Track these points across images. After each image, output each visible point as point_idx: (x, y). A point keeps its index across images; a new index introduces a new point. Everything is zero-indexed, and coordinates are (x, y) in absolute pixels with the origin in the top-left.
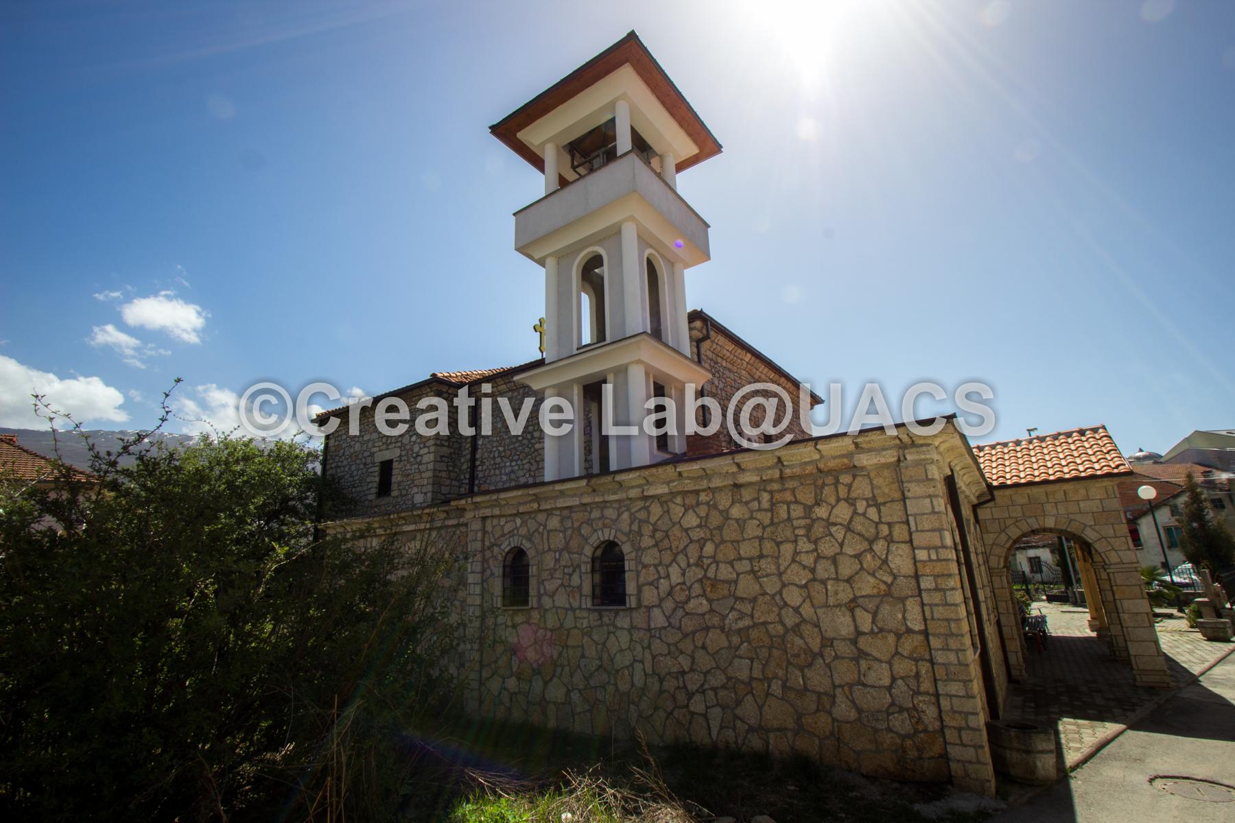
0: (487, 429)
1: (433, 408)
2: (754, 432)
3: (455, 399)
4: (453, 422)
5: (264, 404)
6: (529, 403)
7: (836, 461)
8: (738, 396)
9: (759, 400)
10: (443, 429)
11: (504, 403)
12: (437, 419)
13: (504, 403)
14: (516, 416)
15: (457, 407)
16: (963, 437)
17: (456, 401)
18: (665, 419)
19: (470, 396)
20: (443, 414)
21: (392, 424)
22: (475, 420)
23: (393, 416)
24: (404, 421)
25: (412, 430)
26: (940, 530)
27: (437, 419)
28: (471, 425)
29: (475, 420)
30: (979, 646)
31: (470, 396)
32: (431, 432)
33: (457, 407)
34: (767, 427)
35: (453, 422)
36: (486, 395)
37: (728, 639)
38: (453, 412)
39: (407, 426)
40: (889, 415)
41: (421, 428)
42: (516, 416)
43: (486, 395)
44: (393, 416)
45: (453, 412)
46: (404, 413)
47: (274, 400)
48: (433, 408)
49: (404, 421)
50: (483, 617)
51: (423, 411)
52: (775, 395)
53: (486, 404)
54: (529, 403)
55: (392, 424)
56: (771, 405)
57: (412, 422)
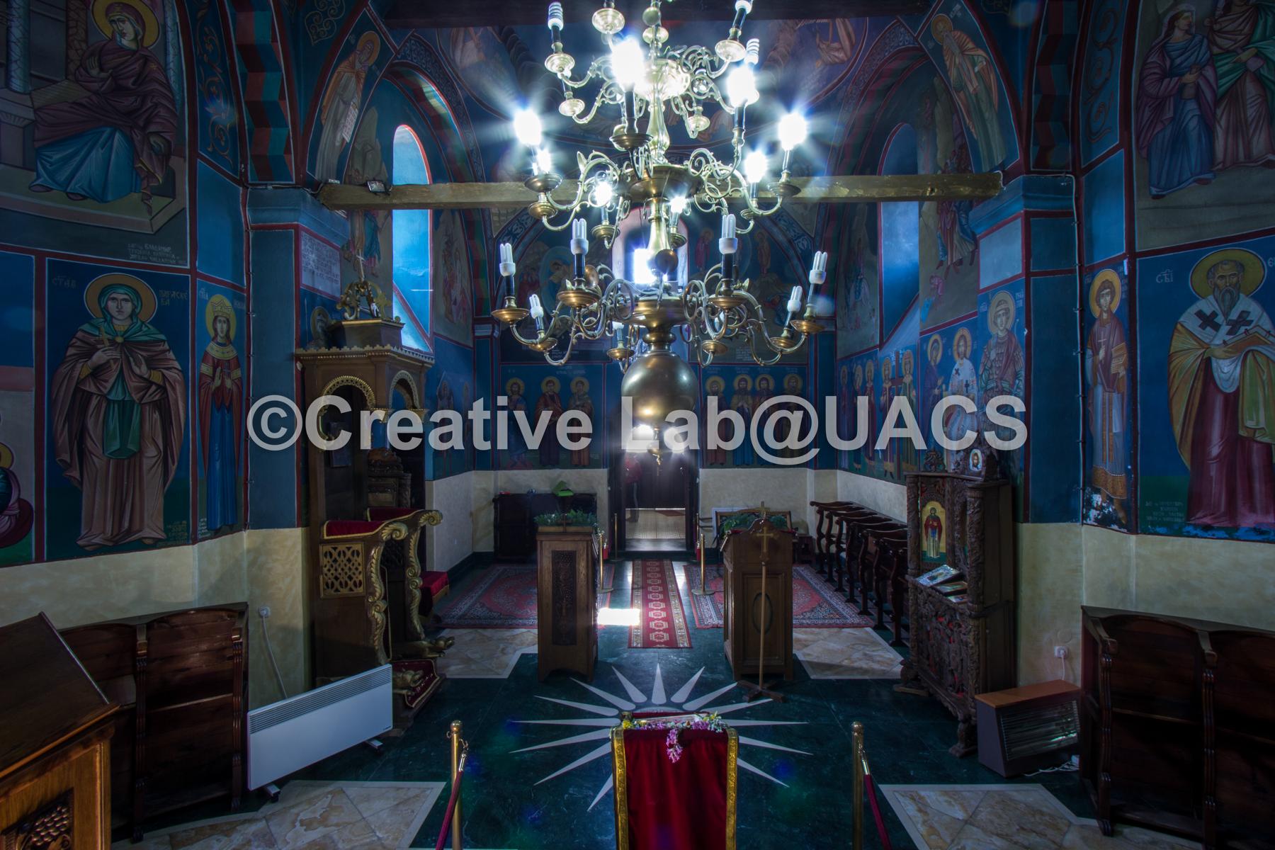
0: (502, 444)
1: (446, 422)
3: (470, 413)
5: (274, 417)
6: (545, 416)
7: (418, 593)
8: (766, 405)
9: (784, 413)
10: (457, 443)
11: (520, 416)
12: (451, 433)
13: (520, 416)
14: (533, 428)
15: (472, 420)
19: (485, 409)
20: (457, 428)
21: (574, 438)
22: (490, 431)
23: (575, 430)
24: (587, 435)
27: (451, 433)
28: (486, 439)
29: (490, 431)
30: (339, 379)
31: (485, 409)
32: (445, 446)
33: (472, 420)
34: (792, 442)
36: (503, 408)
37: (1232, 261)
41: (434, 441)
42: (533, 428)
43: (503, 408)
44: (575, 430)
47: (283, 414)
48: (446, 422)
49: (587, 435)
50: (1113, 480)
51: (436, 425)
52: (799, 407)
53: (502, 417)
55: (574, 438)
56: (796, 418)
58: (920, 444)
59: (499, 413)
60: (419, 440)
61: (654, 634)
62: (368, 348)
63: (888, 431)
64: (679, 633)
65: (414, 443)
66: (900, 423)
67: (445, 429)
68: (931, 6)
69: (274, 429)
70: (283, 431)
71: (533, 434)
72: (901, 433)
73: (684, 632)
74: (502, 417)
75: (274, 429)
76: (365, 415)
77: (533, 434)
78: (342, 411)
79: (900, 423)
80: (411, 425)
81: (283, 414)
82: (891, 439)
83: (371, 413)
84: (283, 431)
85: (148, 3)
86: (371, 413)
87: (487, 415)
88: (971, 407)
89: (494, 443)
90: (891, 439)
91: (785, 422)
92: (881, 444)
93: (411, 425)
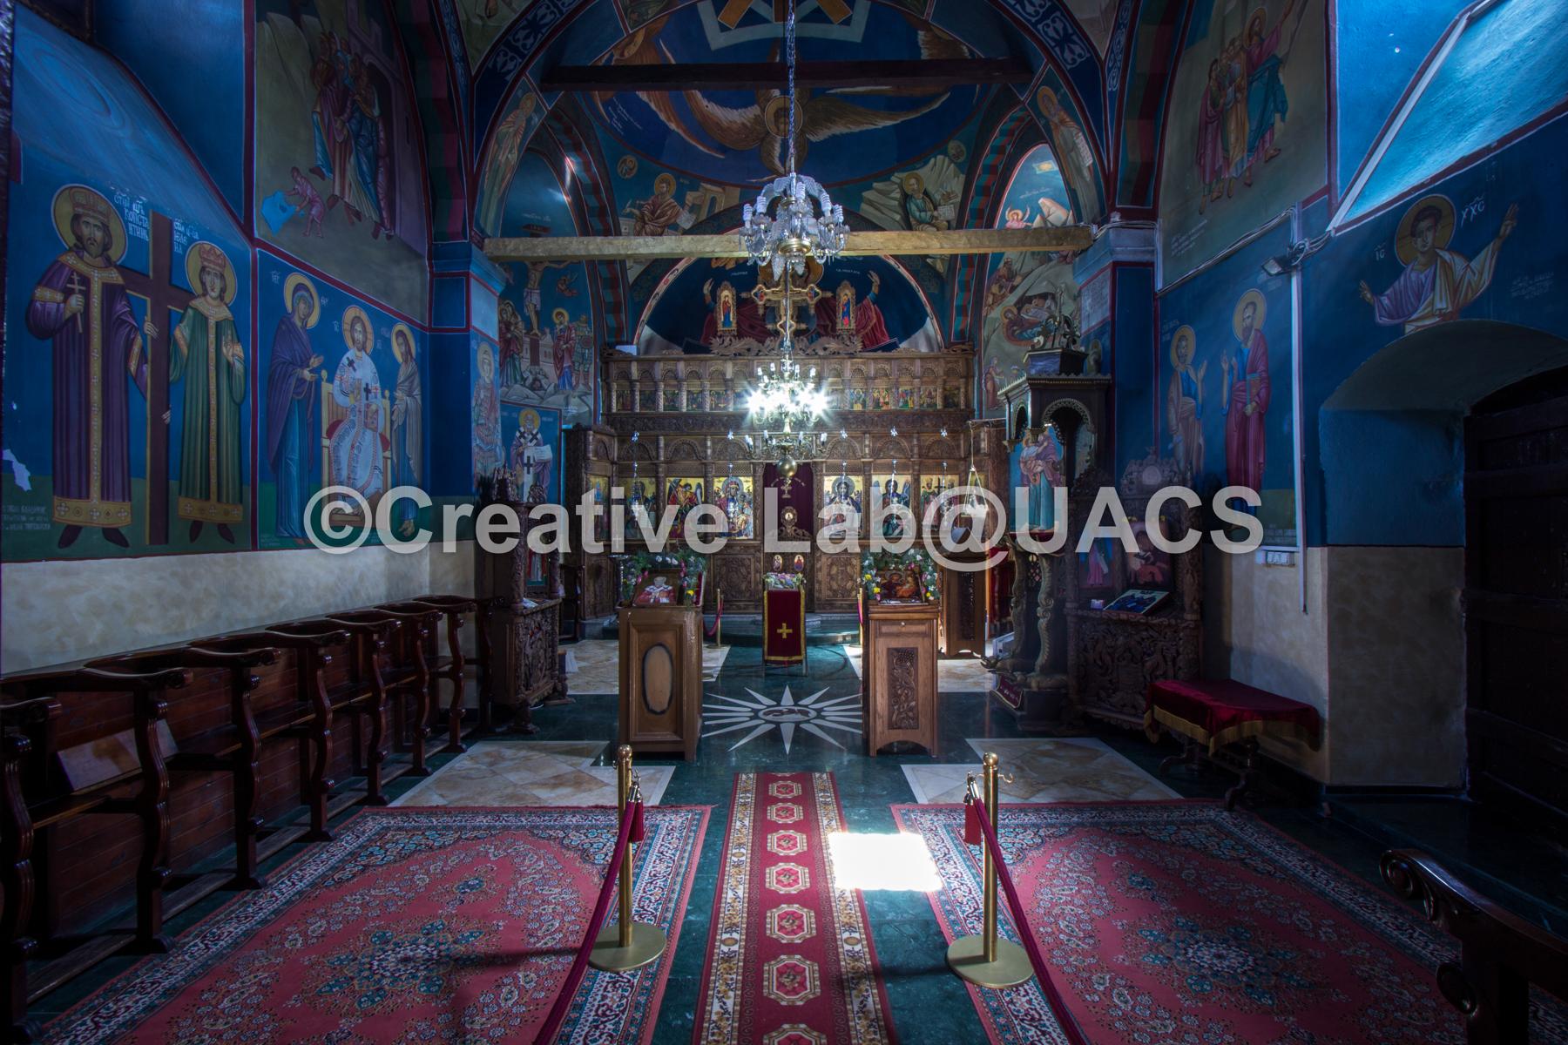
0: (618, 543)
2: (950, 545)
4: (864, 535)
5: (335, 513)
6: (671, 511)
10: (562, 545)
13: (638, 509)
15: (580, 517)
16: (652, 807)
17: (579, 510)
18: (490, 523)
20: (561, 526)
22: (603, 529)
24: (512, 535)
25: (523, 544)
26: (1267, 565)
29: (603, 529)
30: (1087, 413)
33: (580, 517)
35: (864, 535)
38: (575, 524)
39: (517, 540)
40: (283, 424)
42: (656, 530)
44: (710, 528)
45: (575, 524)
46: (514, 525)
48: (550, 518)
53: (617, 511)
54: (671, 511)
55: (498, 538)
57: (522, 536)
58: (1132, 546)
59: (614, 508)
60: (516, 541)
61: (795, 793)
62: (1072, 376)
63: (1093, 530)
64: (750, 798)
65: (509, 545)
66: (1107, 520)
67: (547, 528)
68: (541, 91)
69: (337, 528)
70: (348, 530)
71: (1107, 506)
72: (1106, 533)
73: (741, 798)
74: (617, 511)
75: (337, 528)
76: (448, 510)
77: (1107, 506)
78: (421, 506)
79: (1107, 520)
80: (506, 523)
81: (348, 509)
82: (1096, 541)
83: (456, 508)
84: (348, 530)
85: (28, 2)
86: (456, 508)
87: (600, 510)
88: (1192, 500)
89: (608, 546)
90: (1096, 541)
91: (1174, 509)
92: (1084, 546)
93: (506, 523)
